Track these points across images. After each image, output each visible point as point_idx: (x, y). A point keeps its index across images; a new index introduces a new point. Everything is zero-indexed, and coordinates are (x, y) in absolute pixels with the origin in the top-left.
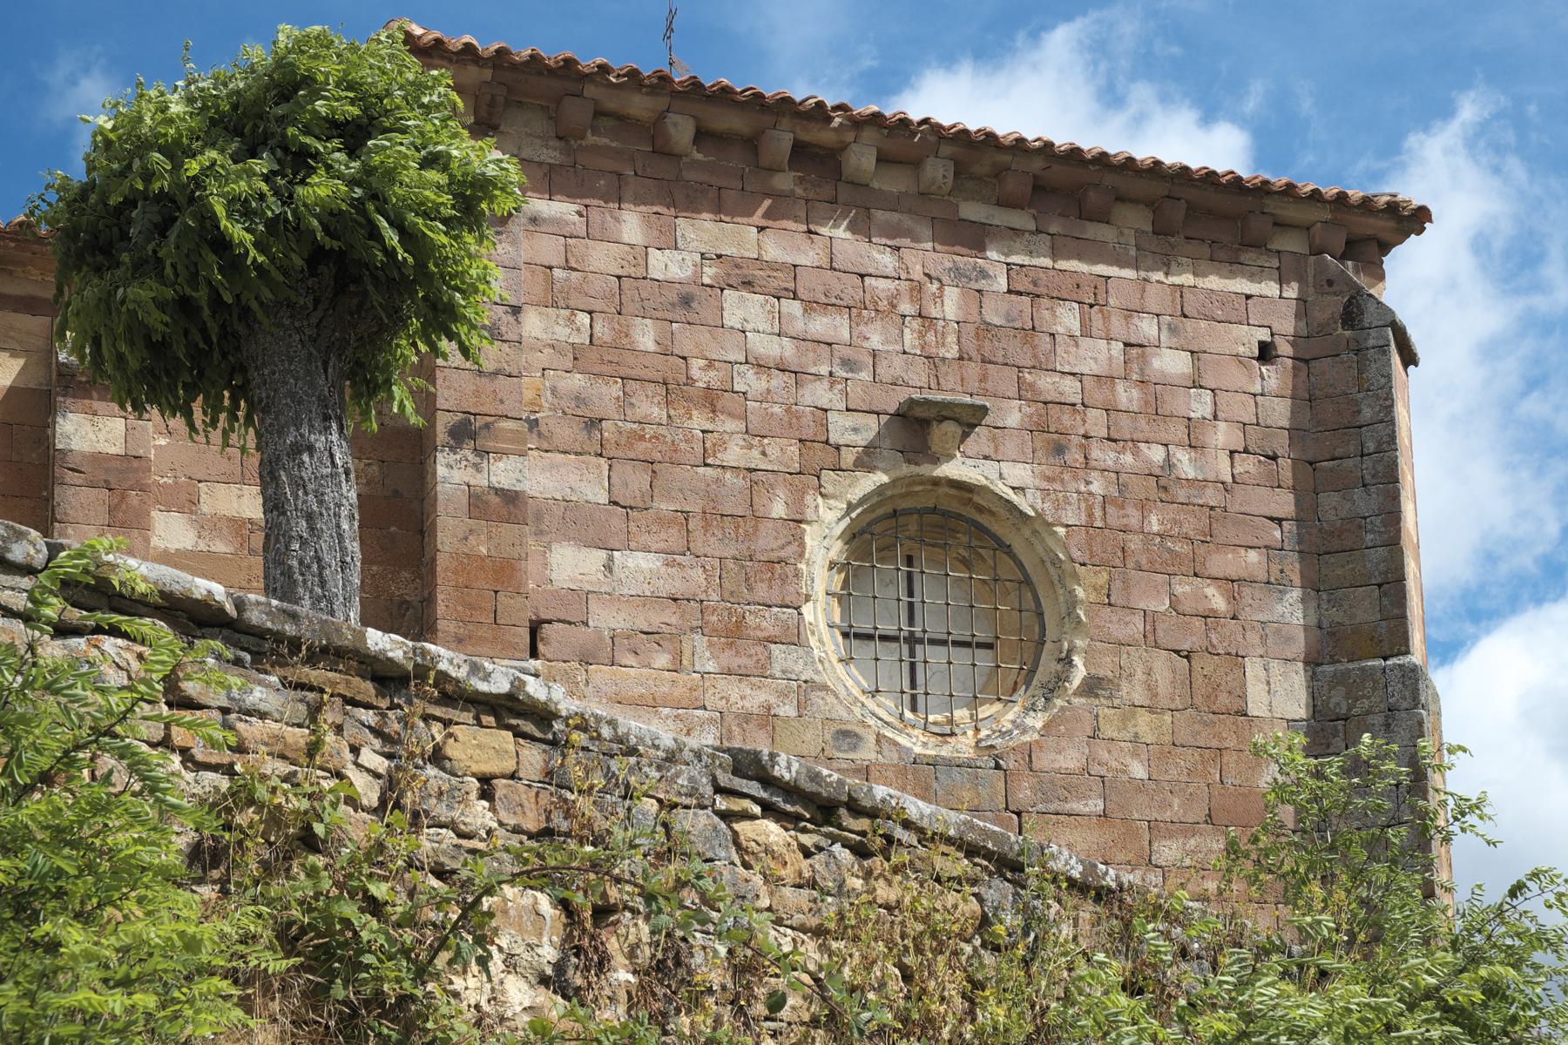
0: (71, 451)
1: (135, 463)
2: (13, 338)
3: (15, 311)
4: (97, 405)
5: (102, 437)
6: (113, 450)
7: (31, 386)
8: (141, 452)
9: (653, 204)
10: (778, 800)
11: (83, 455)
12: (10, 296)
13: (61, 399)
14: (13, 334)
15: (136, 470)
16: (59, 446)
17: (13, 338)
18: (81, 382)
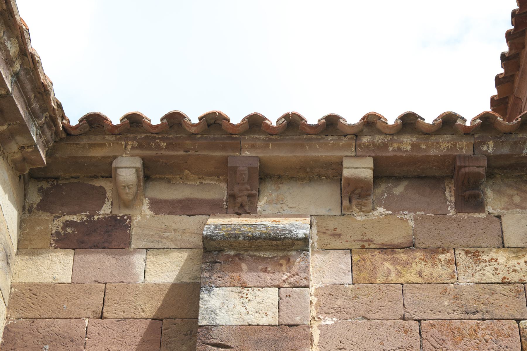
0: (216, 326)
1: (291, 332)
2: (166, 238)
3: (171, 213)
4: (247, 276)
5: (251, 307)
6: (264, 321)
7: (186, 280)
8: (297, 320)
9: (32, 136)
10: (28, 87)
11: (230, 328)
12: (166, 201)
13: (207, 275)
14: (166, 234)
15: (291, 339)
16: (202, 322)
17: (166, 238)
18: (229, 256)
